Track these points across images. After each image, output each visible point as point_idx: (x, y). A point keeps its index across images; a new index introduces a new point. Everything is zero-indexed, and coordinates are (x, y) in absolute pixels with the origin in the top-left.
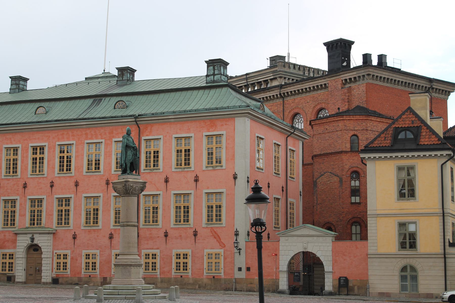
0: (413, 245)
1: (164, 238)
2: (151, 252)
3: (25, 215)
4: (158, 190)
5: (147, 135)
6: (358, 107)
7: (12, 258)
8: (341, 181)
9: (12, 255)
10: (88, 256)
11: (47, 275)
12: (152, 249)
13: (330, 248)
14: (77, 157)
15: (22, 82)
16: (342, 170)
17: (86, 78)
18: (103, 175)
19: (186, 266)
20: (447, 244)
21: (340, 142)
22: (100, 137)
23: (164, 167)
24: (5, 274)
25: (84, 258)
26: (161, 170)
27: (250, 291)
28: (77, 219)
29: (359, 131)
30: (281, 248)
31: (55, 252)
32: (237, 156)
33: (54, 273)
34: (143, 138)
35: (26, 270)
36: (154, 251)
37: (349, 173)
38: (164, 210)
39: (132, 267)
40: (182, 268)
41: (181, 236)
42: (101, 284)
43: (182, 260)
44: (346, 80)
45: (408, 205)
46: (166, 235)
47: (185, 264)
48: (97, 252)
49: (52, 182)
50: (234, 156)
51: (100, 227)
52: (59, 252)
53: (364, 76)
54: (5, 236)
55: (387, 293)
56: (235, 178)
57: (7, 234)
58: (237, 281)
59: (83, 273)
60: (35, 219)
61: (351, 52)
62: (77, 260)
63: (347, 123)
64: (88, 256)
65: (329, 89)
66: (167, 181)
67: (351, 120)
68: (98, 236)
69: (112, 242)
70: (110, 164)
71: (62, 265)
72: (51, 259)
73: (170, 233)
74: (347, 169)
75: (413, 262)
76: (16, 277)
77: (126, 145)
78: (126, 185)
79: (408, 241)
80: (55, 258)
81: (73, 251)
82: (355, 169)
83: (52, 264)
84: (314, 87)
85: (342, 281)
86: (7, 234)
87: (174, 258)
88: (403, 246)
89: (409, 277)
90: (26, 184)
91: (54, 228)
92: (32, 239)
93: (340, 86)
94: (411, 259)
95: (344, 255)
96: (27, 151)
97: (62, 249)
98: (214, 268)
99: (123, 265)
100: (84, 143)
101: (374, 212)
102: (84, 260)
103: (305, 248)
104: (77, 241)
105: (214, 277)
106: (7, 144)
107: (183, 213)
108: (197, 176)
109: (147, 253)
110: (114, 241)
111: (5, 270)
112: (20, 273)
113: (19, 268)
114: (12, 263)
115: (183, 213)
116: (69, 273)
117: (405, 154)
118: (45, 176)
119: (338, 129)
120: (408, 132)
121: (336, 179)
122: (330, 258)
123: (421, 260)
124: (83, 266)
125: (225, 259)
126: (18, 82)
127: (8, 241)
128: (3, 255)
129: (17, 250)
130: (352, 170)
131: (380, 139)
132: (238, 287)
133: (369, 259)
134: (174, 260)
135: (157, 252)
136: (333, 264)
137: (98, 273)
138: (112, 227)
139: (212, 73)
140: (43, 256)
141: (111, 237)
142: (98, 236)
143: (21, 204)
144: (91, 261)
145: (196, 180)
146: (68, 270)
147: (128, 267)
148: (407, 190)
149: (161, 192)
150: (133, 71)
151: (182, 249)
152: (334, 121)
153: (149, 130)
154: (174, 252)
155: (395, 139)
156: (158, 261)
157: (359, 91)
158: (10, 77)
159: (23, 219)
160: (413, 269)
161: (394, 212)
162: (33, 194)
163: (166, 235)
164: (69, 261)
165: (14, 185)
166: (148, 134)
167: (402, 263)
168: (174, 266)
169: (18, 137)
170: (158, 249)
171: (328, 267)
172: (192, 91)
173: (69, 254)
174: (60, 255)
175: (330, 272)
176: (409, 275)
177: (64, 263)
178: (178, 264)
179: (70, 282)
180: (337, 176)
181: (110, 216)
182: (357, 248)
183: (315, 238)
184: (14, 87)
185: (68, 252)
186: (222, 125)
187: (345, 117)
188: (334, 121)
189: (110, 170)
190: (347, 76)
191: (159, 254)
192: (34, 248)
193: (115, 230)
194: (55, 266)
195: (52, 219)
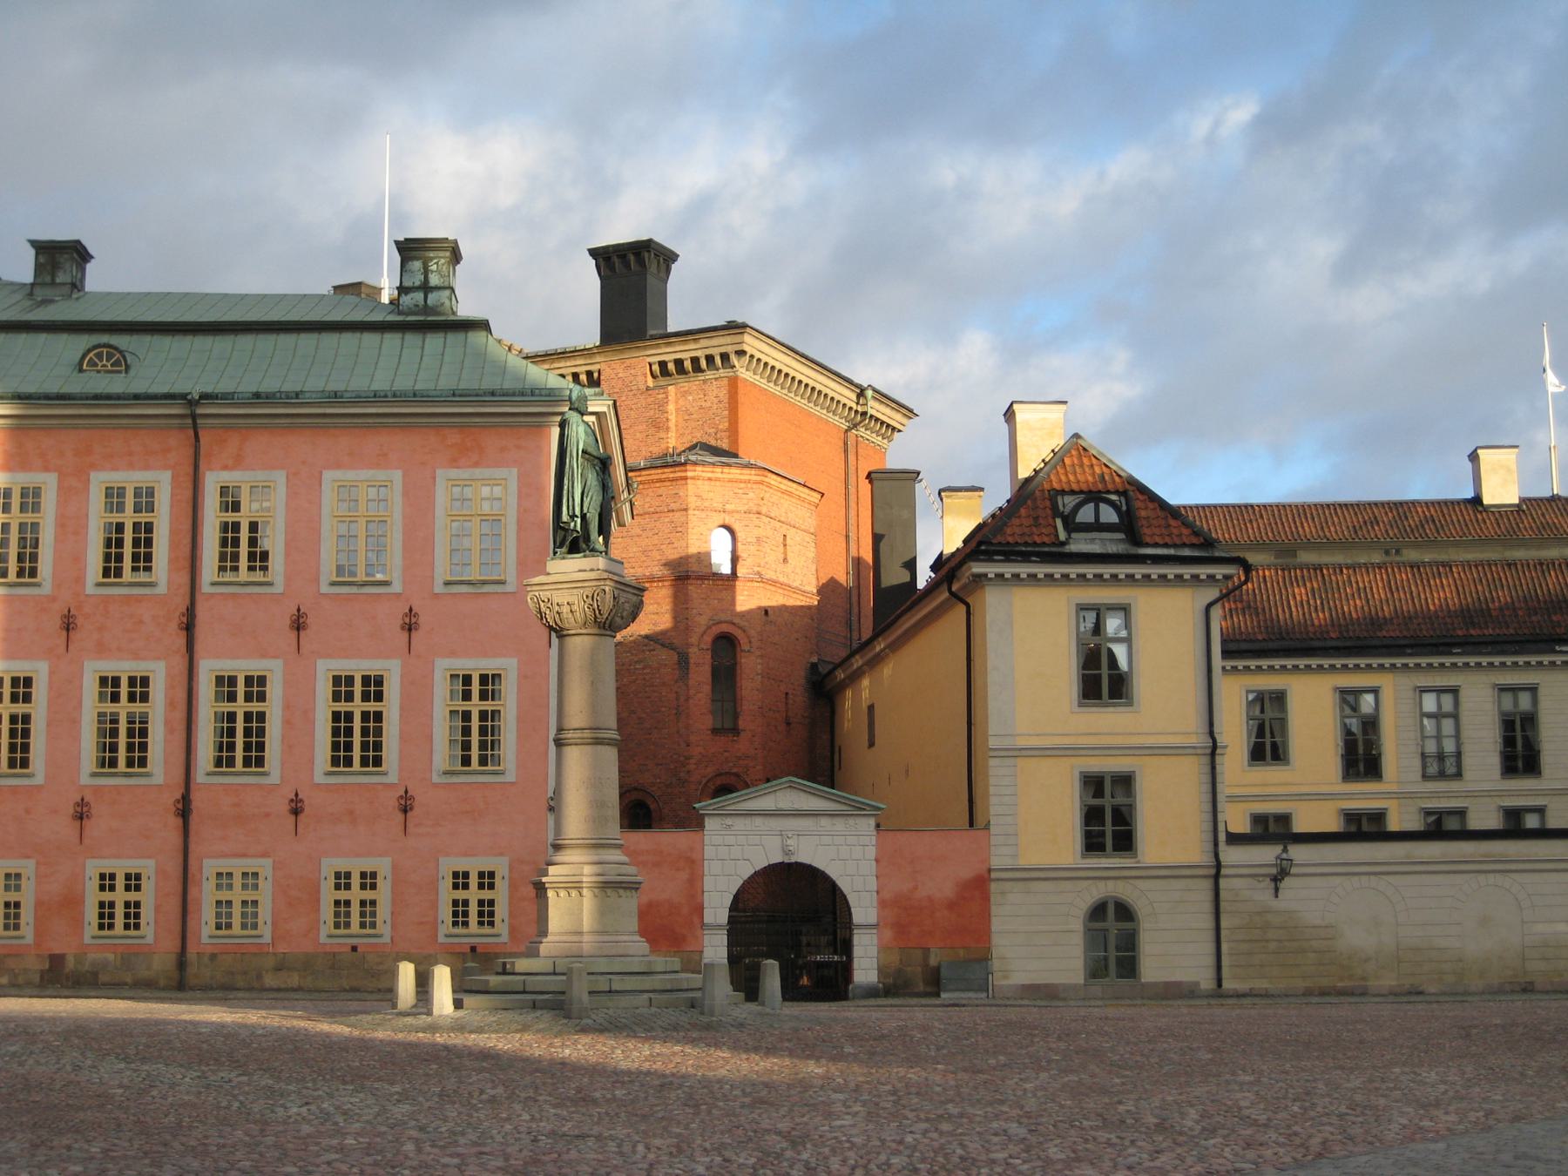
0: (1125, 842)
2: (237, 866)
12: (244, 855)
13: (872, 852)
14: (287, 723)
19: (137, 916)
20: (1222, 837)
23: (288, 579)
26: (279, 588)
29: (737, 516)
30: (709, 852)
36: (251, 864)
37: (708, 639)
40: (119, 920)
41: (351, 813)
42: (42, 978)
45: (1107, 721)
51: (39, 779)
55: (1046, 986)
61: (596, 282)
64: (107, 881)
66: (298, 624)
67: (717, 480)
68: (28, 812)
69: (86, 833)
70: (79, 559)
71: (237, 910)
73: (311, 800)
74: (703, 628)
79: (1108, 819)
84: (695, 360)
88: (1093, 844)
94: (1120, 883)
98: (236, 921)
101: (1007, 743)
105: (473, 949)
107: (357, 741)
109: (133, 871)
110: (98, 826)
115: (357, 741)
119: (673, 506)
120: (1103, 506)
122: (873, 884)
123: (1536, 876)
125: (513, 887)
128: (8, 876)
130: (716, 630)
131: (1015, 521)
134: (328, 895)
138: (85, 779)
139: (417, 283)
141: (81, 814)
142: (28, 812)
144: (120, 896)
145: (410, 628)
148: (1102, 681)
150: (77, 253)
152: (661, 481)
154: (331, 865)
160: (1125, 912)
161: (1067, 741)
166: (230, 462)
170: (264, 855)
171: (863, 910)
172: (358, 335)
176: (1114, 934)
181: (77, 739)
183: (824, 821)
186: (503, 449)
187: (699, 468)
188: (661, 481)
189: (80, 580)
193: (97, 790)
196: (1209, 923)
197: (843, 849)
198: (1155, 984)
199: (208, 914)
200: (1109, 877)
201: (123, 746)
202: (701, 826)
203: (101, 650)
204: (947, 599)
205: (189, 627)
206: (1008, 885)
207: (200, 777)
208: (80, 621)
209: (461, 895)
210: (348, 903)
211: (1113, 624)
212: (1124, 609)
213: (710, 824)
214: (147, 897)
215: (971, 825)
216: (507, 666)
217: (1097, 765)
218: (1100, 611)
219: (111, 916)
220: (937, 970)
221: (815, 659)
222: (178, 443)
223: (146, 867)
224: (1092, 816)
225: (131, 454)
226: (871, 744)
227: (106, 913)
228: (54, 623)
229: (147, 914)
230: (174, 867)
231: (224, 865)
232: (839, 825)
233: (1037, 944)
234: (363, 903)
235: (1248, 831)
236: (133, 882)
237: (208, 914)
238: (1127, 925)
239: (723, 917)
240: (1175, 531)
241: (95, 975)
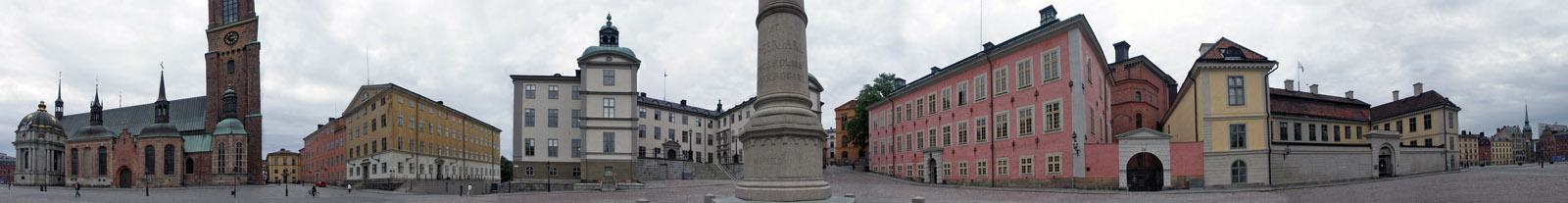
0: (1242, 144)
2: (1002, 159)
8: (1130, 119)
13: (1168, 149)
14: (1011, 124)
27: (1091, 189)
28: (955, 139)
43: (1027, 164)
46: (1014, 145)
47: (1057, 166)
48: (967, 162)
56: (1071, 85)
58: (1076, 180)
66: (1012, 100)
75: (1242, 158)
79: (1238, 139)
88: (1234, 145)
92: (931, 155)
121: (1126, 118)
125: (1064, 160)
132: (1077, 185)
134: (1021, 165)
135: (1007, 159)
141: (975, 150)
144: (1054, 163)
156: (1060, 162)
157: (1135, 72)
159: (927, 145)
160: (1243, 164)
163: (1014, 145)
167: (1234, 159)
168: (1021, 169)
171: (1166, 166)
178: (1024, 167)
192: (932, 161)
196: (1267, 166)
197: (1160, 150)
199: (997, 170)
201: (981, 135)
203: (977, 115)
205: (992, 106)
207: (995, 140)
212: (1241, 77)
213: (1120, 142)
216: (1060, 100)
220: (1188, 182)
224: (1233, 137)
228: (969, 110)
232: (1159, 141)
233: (1218, 172)
235: (1413, 95)
237: (997, 170)
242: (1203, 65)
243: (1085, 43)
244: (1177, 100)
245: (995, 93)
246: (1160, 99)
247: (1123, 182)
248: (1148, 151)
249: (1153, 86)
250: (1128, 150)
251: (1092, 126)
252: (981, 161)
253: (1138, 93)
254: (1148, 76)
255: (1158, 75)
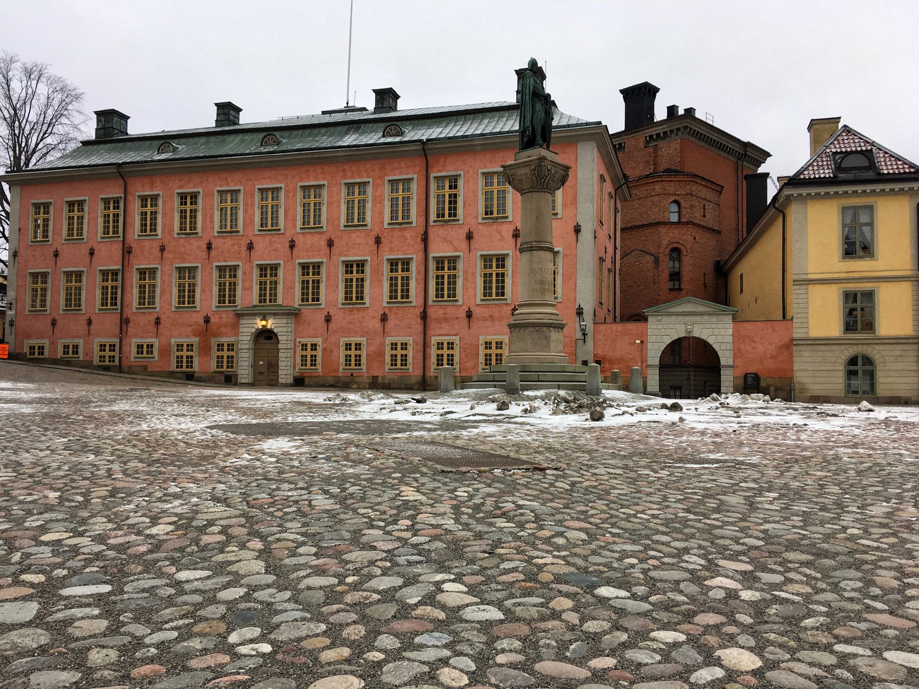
1: (466, 320)
2: (445, 339)
3: (250, 289)
4: (456, 250)
5: (439, 171)
6: (668, 170)
7: (233, 350)
8: (657, 260)
9: (233, 345)
10: (348, 346)
11: (285, 372)
15: (232, 112)
16: (659, 246)
17: (324, 113)
18: (371, 230)
21: (657, 210)
22: (365, 174)
24: (223, 372)
25: (342, 349)
28: (332, 292)
30: (650, 332)
31: (298, 340)
32: (580, 199)
33: (297, 370)
34: (432, 175)
35: (254, 366)
37: (668, 250)
38: (465, 279)
39: (552, 329)
41: (491, 316)
44: (651, 137)
45: (861, 266)
48: (363, 340)
49: (293, 241)
50: (575, 199)
51: (367, 305)
52: (304, 341)
53: (678, 129)
54: (220, 318)
56: (577, 230)
57: (223, 316)
59: (341, 370)
60: (267, 292)
62: (332, 352)
63: (666, 185)
65: (627, 150)
68: (363, 318)
72: (292, 351)
73: (476, 311)
76: (239, 376)
77: (533, 91)
78: (540, 165)
80: (299, 349)
81: (327, 339)
82: (675, 245)
83: (295, 358)
85: (749, 379)
86: (223, 316)
87: (482, 348)
88: (849, 327)
89: (860, 373)
90: (251, 243)
91: (296, 306)
93: (642, 145)
95: (753, 341)
96: (252, 195)
97: (309, 337)
99: (534, 325)
100: (340, 184)
102: (342, 352)
103: (690, 332)
104: (333, 325)
106: (221, 186)
108: (516, 230)
110: (390, 324)
111: (222, 367)
112: (244, 369)
113: (243, 363)
114: (232, 357)
116: (320, 370)
117: (860, 188)
118: (282, 232)
121: (648, 258)
124: (342, 360)
126: (227, 111)
127: (225, 325)
129: (240, 338)
133: (794, 347)
134: (482, 351)
135: (456, 339)
136: (735, 355)
137: (364, 370)
138: (385, 305)
140: (280, 346)
141: (384, 318)
142: (363, 318)
143: (244, 273)
144: (399, 352)
146: (319, 367)
147: (544, 329)
148: (856, 246)
149: (461, 254)
151: (494, 335)
153: (441, 163)
154: (482, 339)
155: (839, 168)
156: (456, 352)
157: (669, 151)
158: (216, 104)
159: (248, 293)
160: (868, 361)
161: (836, 276)
162: (262, 258)
164: (319, 353)
165: (234, 245)
168: (482, 359)
169: (237, 176)
171: (726, 358)
173: (320, 344)
174: (306, 345)
175: (730, 366)
177: (312, 356)
178: (394, 357)
179: (322, 383)
180: (651, 254)
182: (774, 331)
184: (222, 117)
185: (319, 341)
189: (382, 222)
190: (653, 131)
191: (458, 342)
194: (299, 360)
195: (294, 294)
197: (717, 332)
198: (883, 397)
200: (859, 345)
202: (646, 320)
204: (775, 213)
206: (803, 348)
207: (430, 303)
208: (382, 239)
209: (440, 352)
210: (442, 355)
211: (864, 218)
214: (410, 353)
215: (784, 317)
217: (852, 287)
218: (856, 209)
219: (402, 360)
221: (718, 259)
222: (420, 162)
223: (410, 340)
225: (401, 168)
226: (742, 292)
227: (488, 358)
228: (371, 241)
229: (410, 359)
230: (420, 340)
231: (441, 339)
232: (714, 319)
234: (448, 355)
236: (404, 346)
237: (433, 359)
238: (870, 368)
239: (657, 361)
240: (901, 167)
241: (390, 384)
242: (795, 192)
243: (601, 161)
244: (764, 221)
245: (433, 216)
246: (726, 210)
247: (653, 380)
248: (696, 334)
249: (709, 183)
250: (662, 331)
251: (601, 291)
252: (399, 340)
253: (677, 202)
254: (700, 161)
255: (721, 147)
